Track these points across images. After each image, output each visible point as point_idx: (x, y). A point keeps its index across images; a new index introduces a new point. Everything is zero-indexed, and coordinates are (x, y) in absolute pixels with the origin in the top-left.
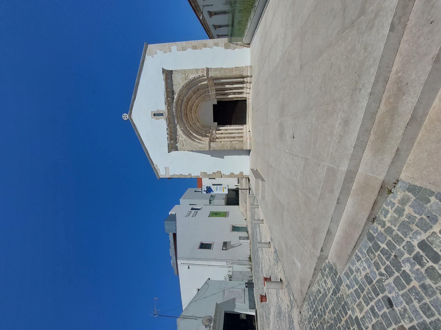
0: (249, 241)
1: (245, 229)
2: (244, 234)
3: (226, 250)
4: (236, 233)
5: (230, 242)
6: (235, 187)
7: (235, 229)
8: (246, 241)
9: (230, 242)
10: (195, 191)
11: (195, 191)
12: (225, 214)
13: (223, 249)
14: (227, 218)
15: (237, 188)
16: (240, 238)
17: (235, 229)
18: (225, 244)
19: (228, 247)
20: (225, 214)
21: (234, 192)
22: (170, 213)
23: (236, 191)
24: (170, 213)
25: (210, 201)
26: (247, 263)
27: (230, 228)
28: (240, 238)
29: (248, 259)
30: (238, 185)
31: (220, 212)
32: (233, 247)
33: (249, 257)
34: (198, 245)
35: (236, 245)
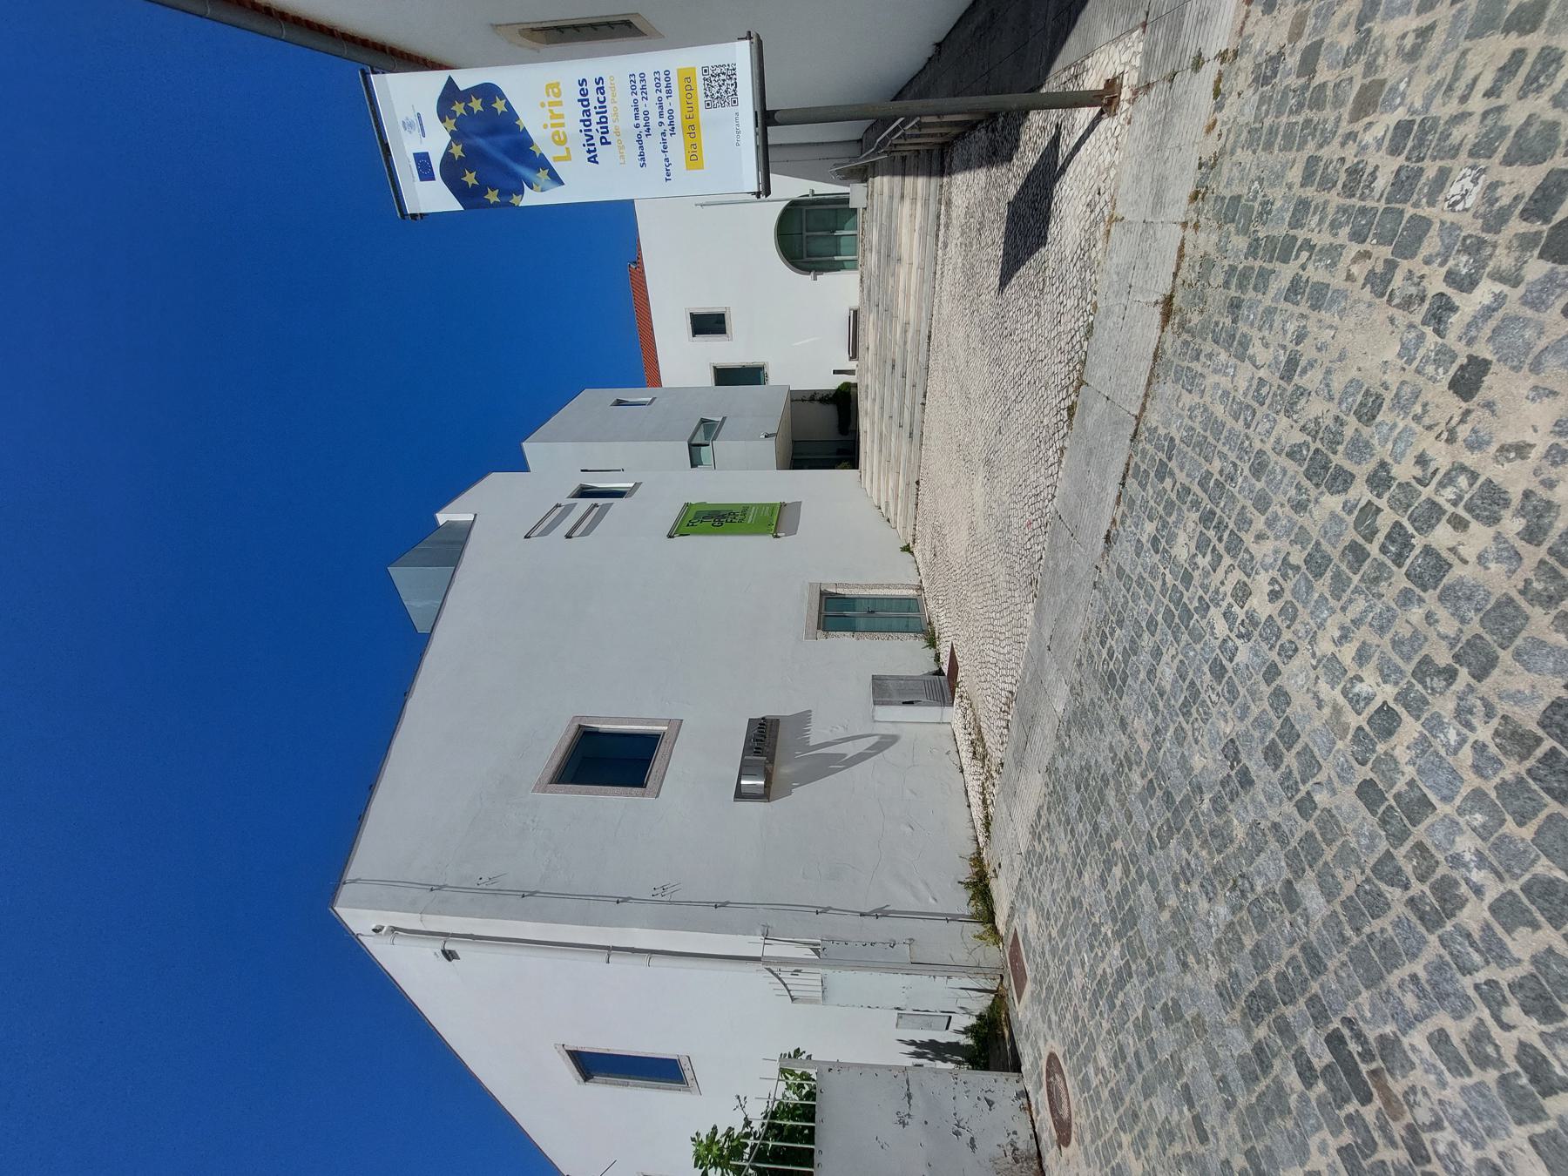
0: (954, 715)
1: (902, 616)
2: (904, 656)
3: (765, 795)
4: (843, 642)
5: (803, 718)
6: (833, 383)
7: (837, 612)
8: (929, 713)
9: (803, 718)
10: (619, 403)
11: (619, 403)
12: (775, 520)
13: (740, 794)
14: (785, 540)
15: (847, 385)
16: (883, 690)
17: (837, 612)
18: (763, 740)
19: (783, 770)
20: (775, 520)
21: (831, 411)
22: (430, 198)
23: (843, 402)
24: (430, 198)
25: (694, 448)
26: (962, 941)
27: (805, 609)
28: (883, 690)
29: (961, 902)
30: (852, 365)
31: (746, 509)
32: (826, 765)
33: (966, 872)
34: (554, 743)
35: (850, 749)
